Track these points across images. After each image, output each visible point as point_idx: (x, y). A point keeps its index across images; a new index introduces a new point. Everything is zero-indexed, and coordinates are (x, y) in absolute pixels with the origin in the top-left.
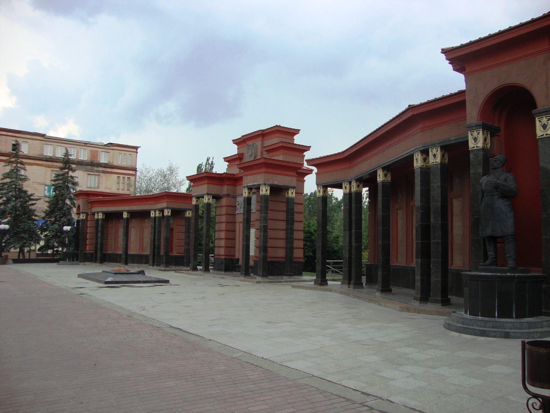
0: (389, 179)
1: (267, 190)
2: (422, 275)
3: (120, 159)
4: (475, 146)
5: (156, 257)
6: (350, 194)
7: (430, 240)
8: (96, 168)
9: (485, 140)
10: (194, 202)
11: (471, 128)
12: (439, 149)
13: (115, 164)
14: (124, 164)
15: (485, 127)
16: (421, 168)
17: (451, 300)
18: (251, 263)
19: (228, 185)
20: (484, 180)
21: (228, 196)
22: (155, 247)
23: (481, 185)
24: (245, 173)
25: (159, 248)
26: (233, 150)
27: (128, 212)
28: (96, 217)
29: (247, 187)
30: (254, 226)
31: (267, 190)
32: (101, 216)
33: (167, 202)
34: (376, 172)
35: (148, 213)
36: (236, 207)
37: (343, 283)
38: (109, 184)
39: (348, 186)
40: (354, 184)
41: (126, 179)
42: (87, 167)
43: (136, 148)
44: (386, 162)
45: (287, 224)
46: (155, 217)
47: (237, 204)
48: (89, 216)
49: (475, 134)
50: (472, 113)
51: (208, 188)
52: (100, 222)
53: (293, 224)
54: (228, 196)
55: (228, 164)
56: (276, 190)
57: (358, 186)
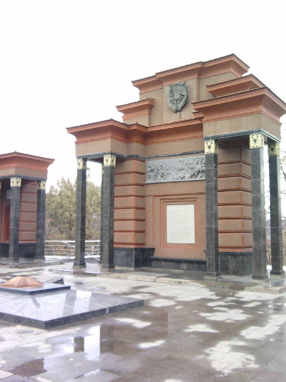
4: (107, 164)
9: (113, 161)
12: (213, 142)
17: (45, 257)
26: (134, 96)
29: (212, 138)
33: (16, 167)
49: (209, 143)
51: (112, 142)
54: (136, 158)
55: (123, 114)
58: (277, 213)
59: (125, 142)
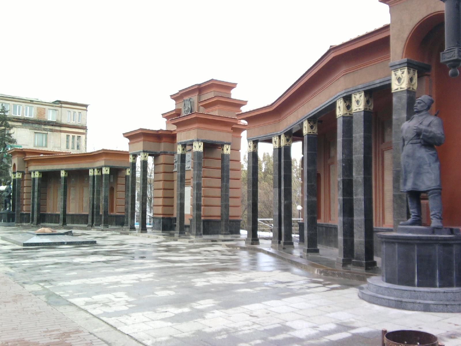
0: (316, 131)
1: (200, 147)
2: (344, 235)
3: (67, 116)
5: (95, 217)
6: (280, 149)
7: (353, 197)
8: (43, 127)
9: (411, 80)
10: (131, 160)
11: (395, 67)
13: (64, 121)
14: (72, 123)
15: (410, 65)
16: (343, 117)
18: (187, 222)
19: (164, 142)
20: (406, 125)
21: (165, 153)
22: (95, 208)
23: (402, 131)
24: (179, 130)
25: (98, 207)
26: (171, 106)
27: (67, 171)
28: (32, 176)
29: (180, 143)
30: (189, 184)
31: (200, 147)
32: (37, 175)
33: (105, 160)
34: (302, 123)
35: (86, 171)
36: (173, 164)
37: (273, 242)
38: (57, 143)
39: (277, 140)
40: (283, 138)
41: (76, 138)
42: (34, 125)
43: (86, 106)
44: (311, 112)
45: (222, 181)
46: (94, 176)
47: (175, 161)
48: (25, 176)
49: (399, 73)
50: (397, 50)
52: (37, 182)
53: (228, 182)
54: (165, 153)
55: (166, 120)
56: (210, 146)
57: (288, 140)
58: (352, 178)
59: (158, 142)
